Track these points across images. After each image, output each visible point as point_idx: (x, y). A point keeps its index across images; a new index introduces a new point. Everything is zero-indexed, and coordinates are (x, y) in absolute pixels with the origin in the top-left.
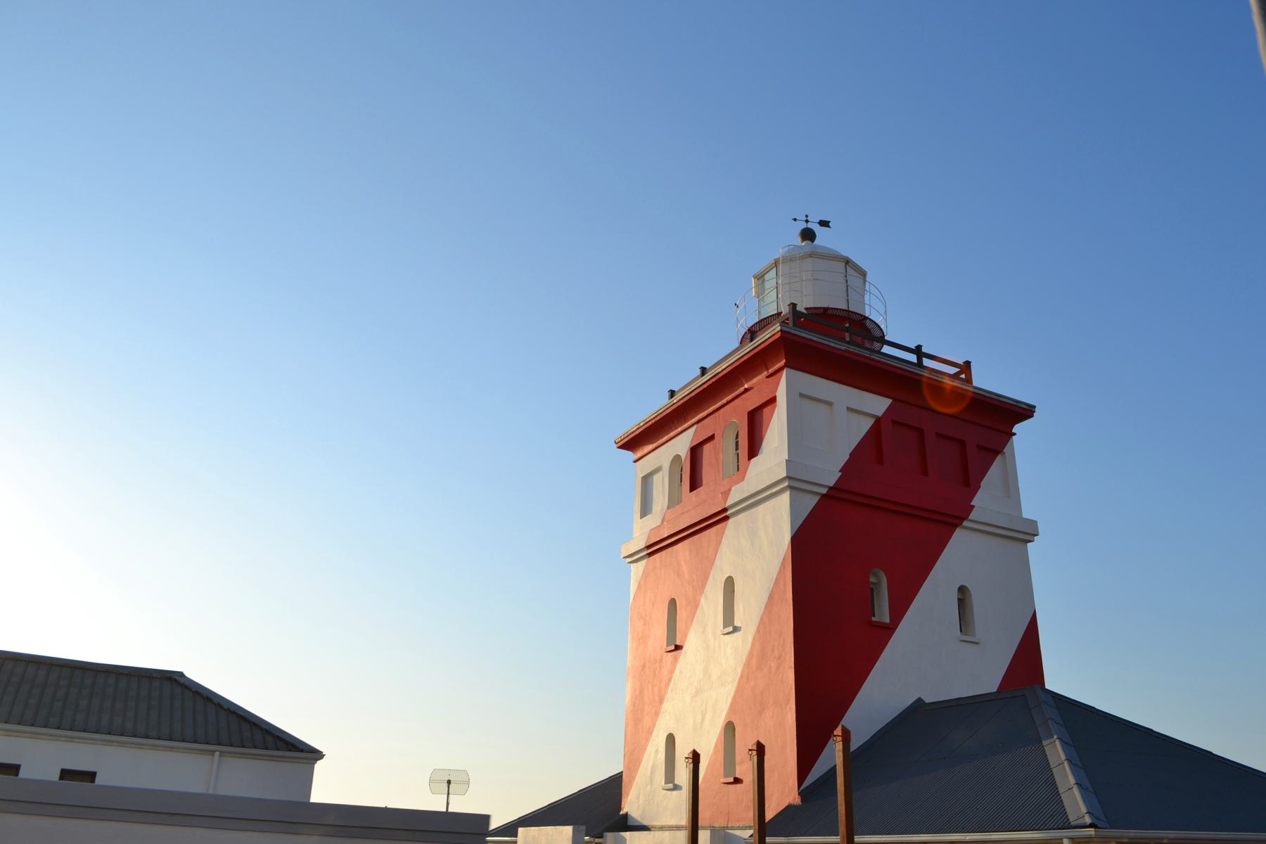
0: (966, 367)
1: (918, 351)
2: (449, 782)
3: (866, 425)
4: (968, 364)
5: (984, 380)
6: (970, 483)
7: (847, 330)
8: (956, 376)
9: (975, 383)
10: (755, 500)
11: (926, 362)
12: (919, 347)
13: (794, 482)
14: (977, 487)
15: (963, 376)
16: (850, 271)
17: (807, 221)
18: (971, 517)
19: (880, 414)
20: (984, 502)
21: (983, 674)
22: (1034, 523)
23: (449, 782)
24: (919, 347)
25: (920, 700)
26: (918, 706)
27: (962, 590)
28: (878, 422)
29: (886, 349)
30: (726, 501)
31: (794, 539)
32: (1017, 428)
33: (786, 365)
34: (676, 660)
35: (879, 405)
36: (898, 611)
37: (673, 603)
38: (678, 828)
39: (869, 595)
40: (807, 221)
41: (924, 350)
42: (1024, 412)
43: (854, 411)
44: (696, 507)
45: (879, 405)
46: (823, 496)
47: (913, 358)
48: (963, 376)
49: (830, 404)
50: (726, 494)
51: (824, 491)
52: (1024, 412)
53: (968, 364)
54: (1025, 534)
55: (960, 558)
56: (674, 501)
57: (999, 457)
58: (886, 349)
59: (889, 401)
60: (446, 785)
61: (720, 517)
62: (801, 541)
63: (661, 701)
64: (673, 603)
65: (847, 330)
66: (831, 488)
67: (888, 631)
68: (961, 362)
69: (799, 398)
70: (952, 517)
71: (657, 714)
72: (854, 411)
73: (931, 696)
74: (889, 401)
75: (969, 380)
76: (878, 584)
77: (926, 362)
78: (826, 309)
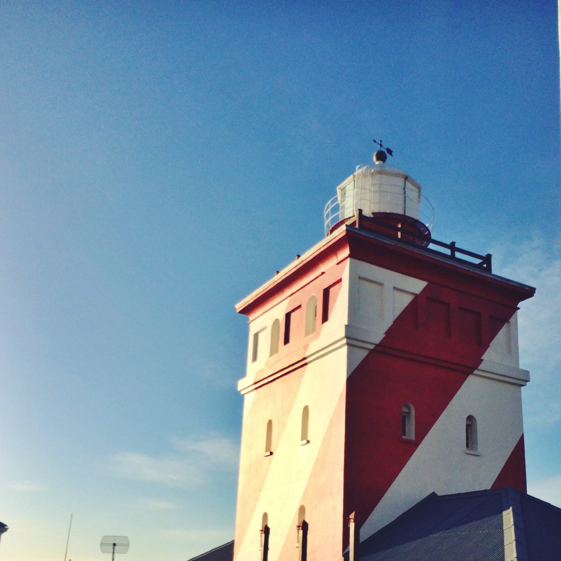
0: (488, 259)
1: (452, 246)
2: (114, 545)
3: (407, 300)
4: (489, 257)
5: (499, 269)
6: (483, 345)
7: (399, 230)
8: (481, 264)
9: (494, 272)
10: (323, 353)
11: (458, 255)
12: (453, 243)
13: (352, 339)
14: (487, 346)
15: (485, 266)
16: (408, 185)
17: (381, 145)
18: (480, 367)
19: (418, 293)
20: (492, 357)
21: (481, 476)
22: (527, 373)
23: (114, 545)
24: (453, 243)
25: (433, 494)
27: (470, 418)
28: (417, 297)
29: (432, 246)
30: (305, 352)
31: (350, 381)
32: (521, 305)
33: (350, 256)
34: (270, 462)
35: (418, 286)
37: (270, 423)
39: (404, 418)
40: (381, 145)
43: (400, 290)
44: (288, 355)
45: (418, 286)
46: (371, 351)
47: (448, 252)
48: (485, 266)
49: (381, 284)
50: (306, 347)
51: (372, 347)
52: (527, 292)
53: (489, 257)
54: (520, 380)
55: (471, 396)
56: (274, 351)
57: (506, 324)
58: (432, 246)
60: (112, 547)
61: (302, 363)
62: (353, 382)
63: (260, 490)
64: (270, 423)
65: (399, 230)
66: (377, 346)
67: (415, 444)
68: (484, 254)
69: (357, 280)
70: (469, 366)
71: (257, 499)
72: (400, 290)
73: (440, 493)
75: (489, 269)
76: (409, 413)
77: (458, 255)
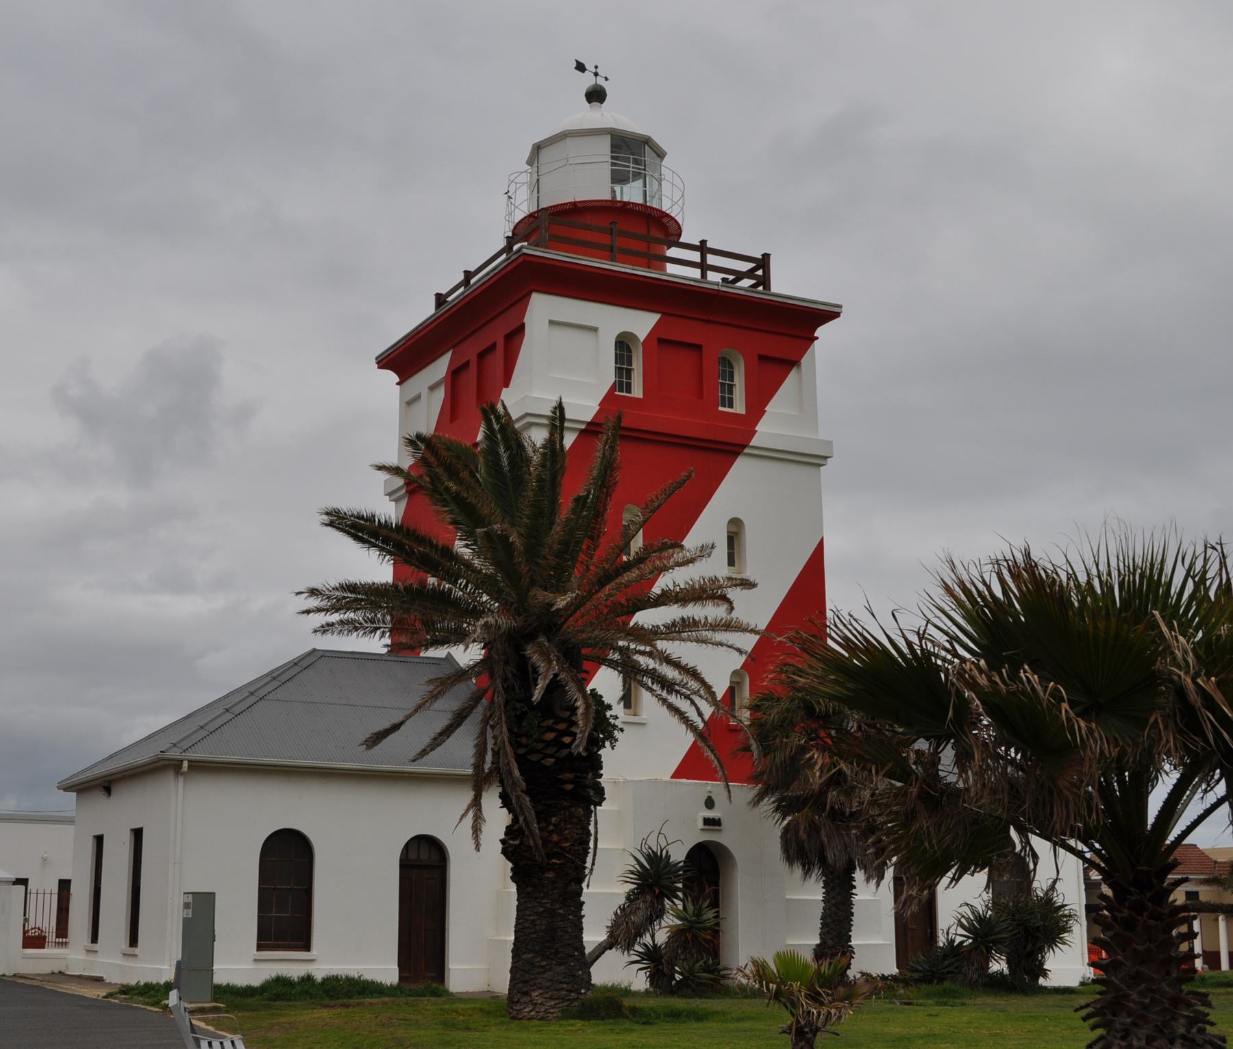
4: (766, 257)
8: (750, 274)
11: (712, 260)
12: (703, 242)
24: (703, 242)
26: (1195, 845)
32: (820, 332)
36: (1035, 865)
38: (739, 651)
41: (709, 245)
42: (828, 314)
45: (642, 323)
46: (582, 432)
51: (583, 427)
52: (828, 314)
53: (766, 257)
55: (739, 491)
57: (792, 376)
59: (656, 317)
66: (589, 424)
74: (656, 317)
75: (765, 281)
78: (574, 204)
